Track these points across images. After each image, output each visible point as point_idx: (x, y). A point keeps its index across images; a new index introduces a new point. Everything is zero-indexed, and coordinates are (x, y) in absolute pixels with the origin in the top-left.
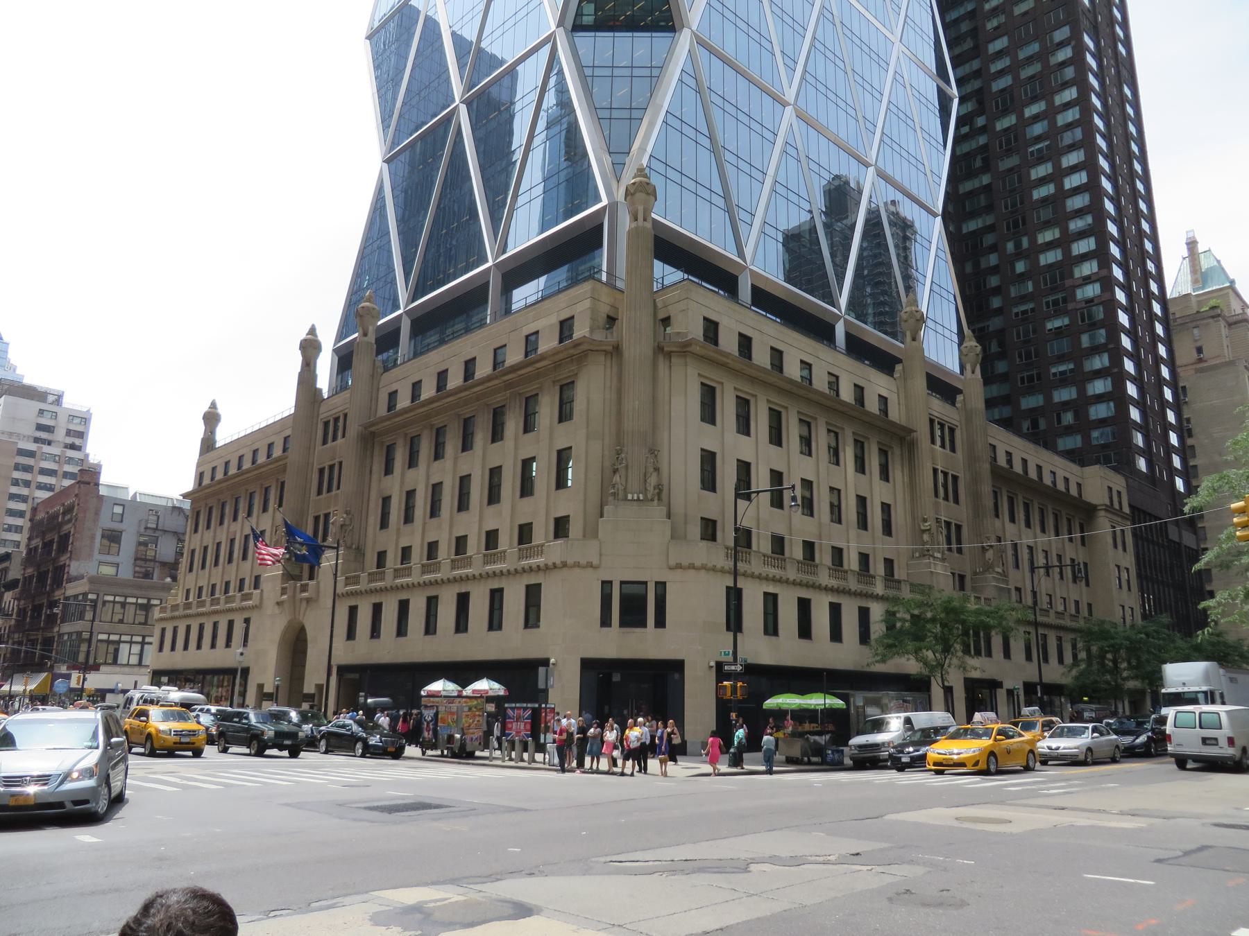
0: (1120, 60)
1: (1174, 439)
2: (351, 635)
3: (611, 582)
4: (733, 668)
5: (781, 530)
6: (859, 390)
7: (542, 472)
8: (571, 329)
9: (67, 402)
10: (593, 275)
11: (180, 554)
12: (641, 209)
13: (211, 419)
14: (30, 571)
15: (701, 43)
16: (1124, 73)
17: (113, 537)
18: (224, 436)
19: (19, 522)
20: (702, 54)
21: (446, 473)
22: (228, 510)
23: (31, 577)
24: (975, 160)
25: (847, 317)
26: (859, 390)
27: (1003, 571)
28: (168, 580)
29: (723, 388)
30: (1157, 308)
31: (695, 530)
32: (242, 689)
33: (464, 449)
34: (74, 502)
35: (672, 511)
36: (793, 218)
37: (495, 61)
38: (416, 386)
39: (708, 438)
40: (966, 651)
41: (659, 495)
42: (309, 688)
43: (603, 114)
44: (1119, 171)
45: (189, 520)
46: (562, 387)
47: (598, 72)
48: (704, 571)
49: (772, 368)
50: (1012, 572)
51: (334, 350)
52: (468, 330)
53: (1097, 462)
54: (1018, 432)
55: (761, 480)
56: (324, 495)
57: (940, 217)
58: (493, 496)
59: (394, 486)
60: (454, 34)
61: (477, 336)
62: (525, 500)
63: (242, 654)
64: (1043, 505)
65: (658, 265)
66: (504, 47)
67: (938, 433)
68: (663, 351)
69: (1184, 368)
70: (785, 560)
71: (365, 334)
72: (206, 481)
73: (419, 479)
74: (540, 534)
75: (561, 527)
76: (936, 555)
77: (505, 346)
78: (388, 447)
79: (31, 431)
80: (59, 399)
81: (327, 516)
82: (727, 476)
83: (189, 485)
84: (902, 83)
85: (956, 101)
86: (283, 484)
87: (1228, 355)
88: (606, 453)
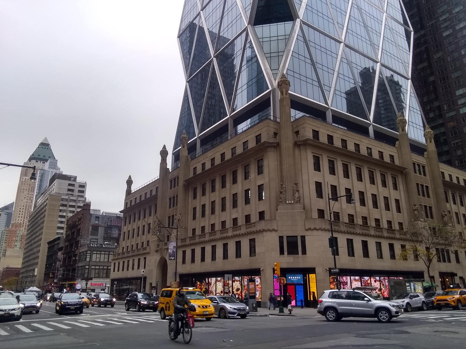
2: (184, 262)
3: (282, 237)
4: (335, 270)
5: (352, 212)
7: (253, 195)
8: (260, 138)
9: (78, 180)
10: (267, 118)
11: (120, 234)
12: (284, 90)
13: (129, 182)
14: (67, 243)
15: (304, 23)
18: (134, 188)
19: (62, 225)
20: (305, 27)
21: (216, 197)
23: (67, 246)
25: (373, 124)
26: (381, 153)
29: (322, 157)
31: (315, 215)
33: (223, 187)
34: (82, 216)
35: (305, 207)
36: (349, 86)
37: (226, 40)
38: (204, 165)
40: (439, 261)
41: (299, 201)
43: (267, 55)
45: (123, 221)
46: (258, 161)
47: (264, 40)
49: (342, 147)
50: (457, 225)
52: (221, 142)
54: (455, 167)
55: (342, 192)
58: (235, 205)
59: (198, 204)
61: (226, 144)
65: (293, 112)
66: (229, 35)
70: (354, 225)
71: (184, 147)
72: (129, 206)
73: (206, 200)
75: (262, 215)
76: (421, 220)
78: (194, 188)
79: (66, 192)
80: (75, 178)
81: (173, 216)
82: (327, 191)
83: (122, 208)
84: (389, 28)
85: (412, 33)
86: (156, 205)
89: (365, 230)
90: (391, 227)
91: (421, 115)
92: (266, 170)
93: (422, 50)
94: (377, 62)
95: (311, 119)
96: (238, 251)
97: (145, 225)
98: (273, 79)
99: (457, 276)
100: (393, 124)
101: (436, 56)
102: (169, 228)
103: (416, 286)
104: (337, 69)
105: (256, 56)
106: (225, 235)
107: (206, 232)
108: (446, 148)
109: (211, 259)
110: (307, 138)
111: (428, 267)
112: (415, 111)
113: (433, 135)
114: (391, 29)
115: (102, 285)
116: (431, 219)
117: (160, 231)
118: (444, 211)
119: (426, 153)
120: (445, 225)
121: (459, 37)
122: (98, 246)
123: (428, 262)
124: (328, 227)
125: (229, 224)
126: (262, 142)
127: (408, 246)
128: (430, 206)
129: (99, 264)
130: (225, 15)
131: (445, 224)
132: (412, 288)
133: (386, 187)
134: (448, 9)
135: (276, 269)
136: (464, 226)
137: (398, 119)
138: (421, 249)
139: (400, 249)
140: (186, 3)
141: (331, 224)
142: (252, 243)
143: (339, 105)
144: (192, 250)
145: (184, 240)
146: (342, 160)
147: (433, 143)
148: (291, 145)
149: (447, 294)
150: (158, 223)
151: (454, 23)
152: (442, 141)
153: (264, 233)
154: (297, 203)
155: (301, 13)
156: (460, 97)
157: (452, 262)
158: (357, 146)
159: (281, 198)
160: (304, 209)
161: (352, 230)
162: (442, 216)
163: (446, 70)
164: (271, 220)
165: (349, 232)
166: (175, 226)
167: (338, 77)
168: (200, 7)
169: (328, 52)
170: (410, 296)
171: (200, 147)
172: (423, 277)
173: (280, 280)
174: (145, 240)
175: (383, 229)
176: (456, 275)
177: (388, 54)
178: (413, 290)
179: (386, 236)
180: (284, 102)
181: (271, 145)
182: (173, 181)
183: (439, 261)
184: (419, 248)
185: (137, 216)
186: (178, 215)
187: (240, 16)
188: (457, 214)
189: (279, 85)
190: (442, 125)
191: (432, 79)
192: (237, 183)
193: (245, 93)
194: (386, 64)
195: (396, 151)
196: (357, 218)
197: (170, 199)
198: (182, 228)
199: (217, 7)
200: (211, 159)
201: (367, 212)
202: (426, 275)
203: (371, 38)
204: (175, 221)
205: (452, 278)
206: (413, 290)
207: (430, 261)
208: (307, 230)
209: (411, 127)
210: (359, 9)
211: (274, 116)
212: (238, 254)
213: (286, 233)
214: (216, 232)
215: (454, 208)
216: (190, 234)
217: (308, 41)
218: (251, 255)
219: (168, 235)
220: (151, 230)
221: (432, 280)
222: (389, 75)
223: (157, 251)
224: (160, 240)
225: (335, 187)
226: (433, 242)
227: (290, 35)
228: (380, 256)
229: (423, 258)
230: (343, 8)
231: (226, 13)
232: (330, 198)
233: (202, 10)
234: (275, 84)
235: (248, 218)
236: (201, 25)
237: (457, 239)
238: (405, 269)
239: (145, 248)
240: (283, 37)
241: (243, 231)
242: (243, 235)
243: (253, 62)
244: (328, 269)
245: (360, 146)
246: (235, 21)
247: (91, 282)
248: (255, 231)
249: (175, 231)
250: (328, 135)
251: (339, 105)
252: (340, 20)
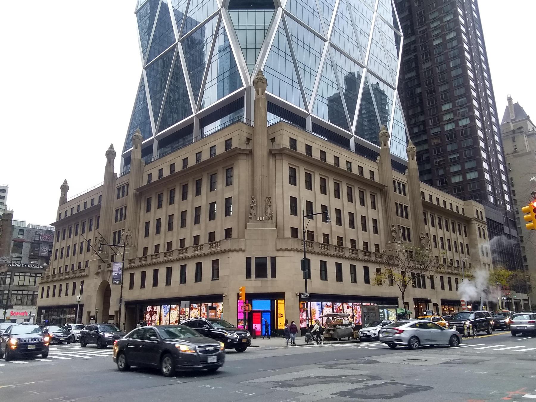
0: (474, 19)
1: (505, 188)
4: (305, 295)
6: (361, 169)
10: (240, 120)
11: (50, 252)
13: (65, 188)
15: (287, 13)
16: (476, 25)
17: (19, 244)
18: (71, 196)
22: (73, 230)
24: (412, 64)
25: (355, 136)
26: (361, 169)
27: (430, 249)
28: (45, 264)
29: (299, 169)
30: (495, 129)
32: (80, 314)
36: (331, 92)
38: (161, 171)
39: (292, 191)
42: (112, 313)
43: (243, 46)
44: (476, 68)
47: (240, 27)
48: (292, 251)
49: (321, 160)
51: (122, 155)
52: (184, 145)
53: (472, 198)
55: (317, 209)
56: (118, 222)
57: (396, 90)
58: (197, 220)
59: (152, 218)
60: (175, 11)
61: (189, 148)
62: (212, 221)
63: (80, 298)
64: (447, 218)
66: (199, 16)
67: (397, 187)
68: (272, 154)
69: (507, 156)
74: (218, 238)
75: (228, 233)
77: (201, 152)
81: (120, 232)
82: (302, 207)
83: (54, 219)
85: (402, 38)
87: (528, 149)
88: (248, 199)
115: (25, 314)
122: (22, 266)
129: (22, 288)
144: (142, 272)
208: (278, 250)
217: (290, 35)
235: (212, 236)
238: (379, 295)
247: (11, 311)
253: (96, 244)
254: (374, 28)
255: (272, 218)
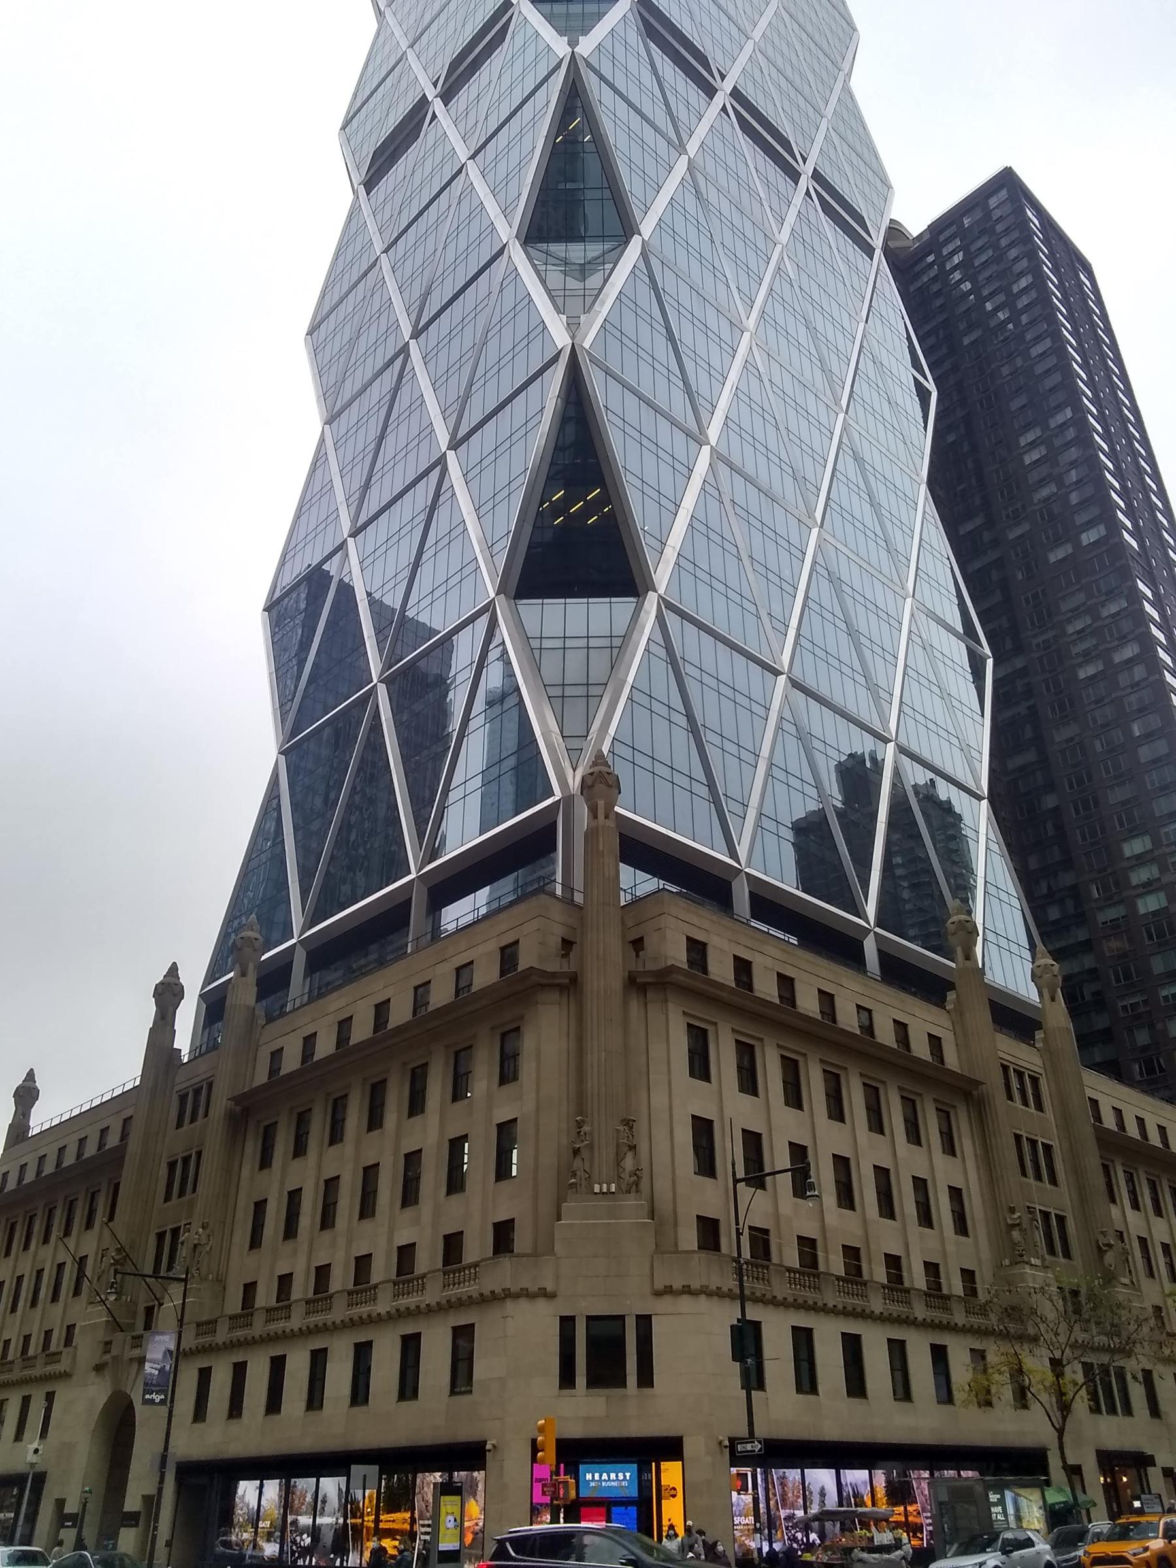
2: (200, 1414)
3: (572, 1319)
4: (749, 1447)
5: (811, 1231)
10: (543, 887)
12: (601, 804)
13: (26, 1095)
18: (41, 1118)
20: (672, 620)
31: (689, 1237)
36: (802, 806)
38: (310, 1041)
46: (504, 1036)
47: (547, 644)
49: (781, 1002)
50: (1145, 1282)
51: (200, 995)
52: (382, 963)
55: (778, 1157)
71: (243, 974)
75: (503, 1235)
76: (1033, 1261)
81: (175, 1232)
85: (990, 663)
86: (117, 1187)
89: (853, 1295)
90: (939, 1287)
91: (1022, 910)
92: (527, 1068)
93: (1019, 713)
94: (886, 741)
95: (682, 902)
96: (410, 1372)
97: (65, 1263)
98: (566, 765)
99: (1155, 1466)
100: (938, 934)
101: (1061, 735)
102: (156, 1278)
103: (1023, 1502)
104: (765, 752)
105: (518, 689)
106: (364, 1310)
107: (294, 1297)
108: (1101, 1022)
109: (303, 1405)
110: (669, 963)
111: (1061, 1432)
112: (1003, 896)
113: (1060, 978)
114: (927, 647)
116: (1063, 1260)
117: (121, 1287)
118: (1102, 1233)
119: (1039, 1035)
120: (1109, 1281)
121: (1122, 685)
123: (1059, 1414)
124: (731, 1283)
125: (382, 1269)
126: (519, 970)
127: (995, 1353)
128: (1062, 1213)
130: (425, 557)
131: (1109, 1278)
132: (1011, 1510)
133: (919, 1143)
134: (1088, 603)
135: (543, 1442)
136: (1168, 1286)
137: (949, 921)
138: (1037, 1364)
139: (968, 1365)
140: (304, 509)
141: (740, 1273)
142: (461, 1342)
143: (773, 864)
145: (207, 1327)
146: (781, 1043)
147: (1060, 1004)
148: (617, 984)
149: (1123, 1534)
150: (117, 1257)
151: (1108, 646)
152: (1088, 997)
153: (509, 1304)
154: (628, 1192)
155: (662, 576)
156: (1134, 862)
157: (1135, 1413)
158: (827, 999)
159: (574, 1175)
160: (652, 1214)
161: (810, 1296)
162: (1099, 1248)
163: (1090, 779)
164: (535, 1254)
165: (800, 1301)
166: (178, 1271)
167: (769, 775)
168: (346, 526)
169: (740, 699)
170: (1003, 1542)
171: (305, 978)
172: (1045, 1471)
173: (554, 1485)
174: (58, 1322)
175: (912, 1291)
176: (1148, 1461)
177: (919, 717)
178: (1011, 1518)
179: (920, 1318)
180: (598, 841)
181: (551, 981)
182: (191, 1095)
183: (1095, 1410)
184: (1029, 1363)
185: (38, 1227)
186: (196, 1227)
187: (472, 567)
188: (1143, 1241)
189: (585, 785)
190: (1087, 946)
191: (1050, 801)
192: (423, 1111)
193: (475, 801)
194: (914, 748)
195: (948, 1024)
196: (826, 1252)
197: (172, 1166)
198: (206, 1279)
199: (403, 532)
200: (339, 1022)
201: (859, 1232)
202: (1054, 1462)
203: (868, 669)
204: (183, 1252)
205: (1138, 1471)
206: (1011, 1518)
207: (1065, 1408)
208: (658, 1294)
209: (993, 949)
210: (834, 580)
211: (568, 886)
212: (408, 1388)
213: (585, 1307)
214: (331, 1297)
215: (1135, 1222)
216: (234, 1304)
218: (457, 1390)
219: (151, 1304)
220: (86, 1284)
221: (1076, 1478)
222: (921, 782)
223: (99, 1368)
224: (115, 1325)
225: (758, 1136)
226: (1072, 1339)
227: (626, 637)
228: (903, 1391)
229: (1044, 1397)
230: (786, 574)
231: (431, 552)
232: (738, 1177)
233: (354, 535)
234: (574, 781)
235: (453, 1244)
236: (346, 580)
237: (1145, 1329)
239: (54, 1354)
240: (605, 642)
241: (432, 1295)
242: (430, 1311)
243: (506, 707)
244: (727, 1443)
245: (837, 999)
246: (457, 578)
248: (475, 1295)
249: (176, 1290)
250: (735, 956)
251: (773, 864)
252: (777, 610)
253: (103, 1271)
254: (909, 638)
255: (637, 1185)
